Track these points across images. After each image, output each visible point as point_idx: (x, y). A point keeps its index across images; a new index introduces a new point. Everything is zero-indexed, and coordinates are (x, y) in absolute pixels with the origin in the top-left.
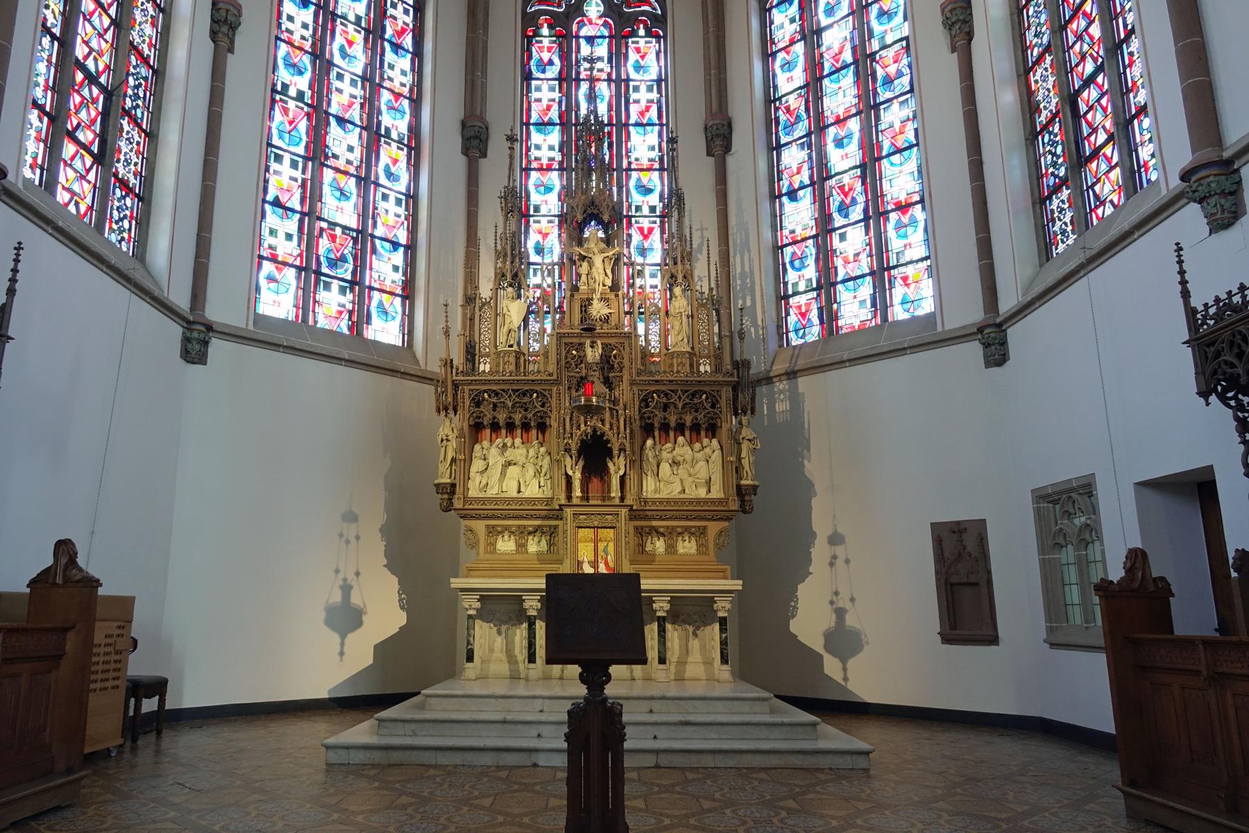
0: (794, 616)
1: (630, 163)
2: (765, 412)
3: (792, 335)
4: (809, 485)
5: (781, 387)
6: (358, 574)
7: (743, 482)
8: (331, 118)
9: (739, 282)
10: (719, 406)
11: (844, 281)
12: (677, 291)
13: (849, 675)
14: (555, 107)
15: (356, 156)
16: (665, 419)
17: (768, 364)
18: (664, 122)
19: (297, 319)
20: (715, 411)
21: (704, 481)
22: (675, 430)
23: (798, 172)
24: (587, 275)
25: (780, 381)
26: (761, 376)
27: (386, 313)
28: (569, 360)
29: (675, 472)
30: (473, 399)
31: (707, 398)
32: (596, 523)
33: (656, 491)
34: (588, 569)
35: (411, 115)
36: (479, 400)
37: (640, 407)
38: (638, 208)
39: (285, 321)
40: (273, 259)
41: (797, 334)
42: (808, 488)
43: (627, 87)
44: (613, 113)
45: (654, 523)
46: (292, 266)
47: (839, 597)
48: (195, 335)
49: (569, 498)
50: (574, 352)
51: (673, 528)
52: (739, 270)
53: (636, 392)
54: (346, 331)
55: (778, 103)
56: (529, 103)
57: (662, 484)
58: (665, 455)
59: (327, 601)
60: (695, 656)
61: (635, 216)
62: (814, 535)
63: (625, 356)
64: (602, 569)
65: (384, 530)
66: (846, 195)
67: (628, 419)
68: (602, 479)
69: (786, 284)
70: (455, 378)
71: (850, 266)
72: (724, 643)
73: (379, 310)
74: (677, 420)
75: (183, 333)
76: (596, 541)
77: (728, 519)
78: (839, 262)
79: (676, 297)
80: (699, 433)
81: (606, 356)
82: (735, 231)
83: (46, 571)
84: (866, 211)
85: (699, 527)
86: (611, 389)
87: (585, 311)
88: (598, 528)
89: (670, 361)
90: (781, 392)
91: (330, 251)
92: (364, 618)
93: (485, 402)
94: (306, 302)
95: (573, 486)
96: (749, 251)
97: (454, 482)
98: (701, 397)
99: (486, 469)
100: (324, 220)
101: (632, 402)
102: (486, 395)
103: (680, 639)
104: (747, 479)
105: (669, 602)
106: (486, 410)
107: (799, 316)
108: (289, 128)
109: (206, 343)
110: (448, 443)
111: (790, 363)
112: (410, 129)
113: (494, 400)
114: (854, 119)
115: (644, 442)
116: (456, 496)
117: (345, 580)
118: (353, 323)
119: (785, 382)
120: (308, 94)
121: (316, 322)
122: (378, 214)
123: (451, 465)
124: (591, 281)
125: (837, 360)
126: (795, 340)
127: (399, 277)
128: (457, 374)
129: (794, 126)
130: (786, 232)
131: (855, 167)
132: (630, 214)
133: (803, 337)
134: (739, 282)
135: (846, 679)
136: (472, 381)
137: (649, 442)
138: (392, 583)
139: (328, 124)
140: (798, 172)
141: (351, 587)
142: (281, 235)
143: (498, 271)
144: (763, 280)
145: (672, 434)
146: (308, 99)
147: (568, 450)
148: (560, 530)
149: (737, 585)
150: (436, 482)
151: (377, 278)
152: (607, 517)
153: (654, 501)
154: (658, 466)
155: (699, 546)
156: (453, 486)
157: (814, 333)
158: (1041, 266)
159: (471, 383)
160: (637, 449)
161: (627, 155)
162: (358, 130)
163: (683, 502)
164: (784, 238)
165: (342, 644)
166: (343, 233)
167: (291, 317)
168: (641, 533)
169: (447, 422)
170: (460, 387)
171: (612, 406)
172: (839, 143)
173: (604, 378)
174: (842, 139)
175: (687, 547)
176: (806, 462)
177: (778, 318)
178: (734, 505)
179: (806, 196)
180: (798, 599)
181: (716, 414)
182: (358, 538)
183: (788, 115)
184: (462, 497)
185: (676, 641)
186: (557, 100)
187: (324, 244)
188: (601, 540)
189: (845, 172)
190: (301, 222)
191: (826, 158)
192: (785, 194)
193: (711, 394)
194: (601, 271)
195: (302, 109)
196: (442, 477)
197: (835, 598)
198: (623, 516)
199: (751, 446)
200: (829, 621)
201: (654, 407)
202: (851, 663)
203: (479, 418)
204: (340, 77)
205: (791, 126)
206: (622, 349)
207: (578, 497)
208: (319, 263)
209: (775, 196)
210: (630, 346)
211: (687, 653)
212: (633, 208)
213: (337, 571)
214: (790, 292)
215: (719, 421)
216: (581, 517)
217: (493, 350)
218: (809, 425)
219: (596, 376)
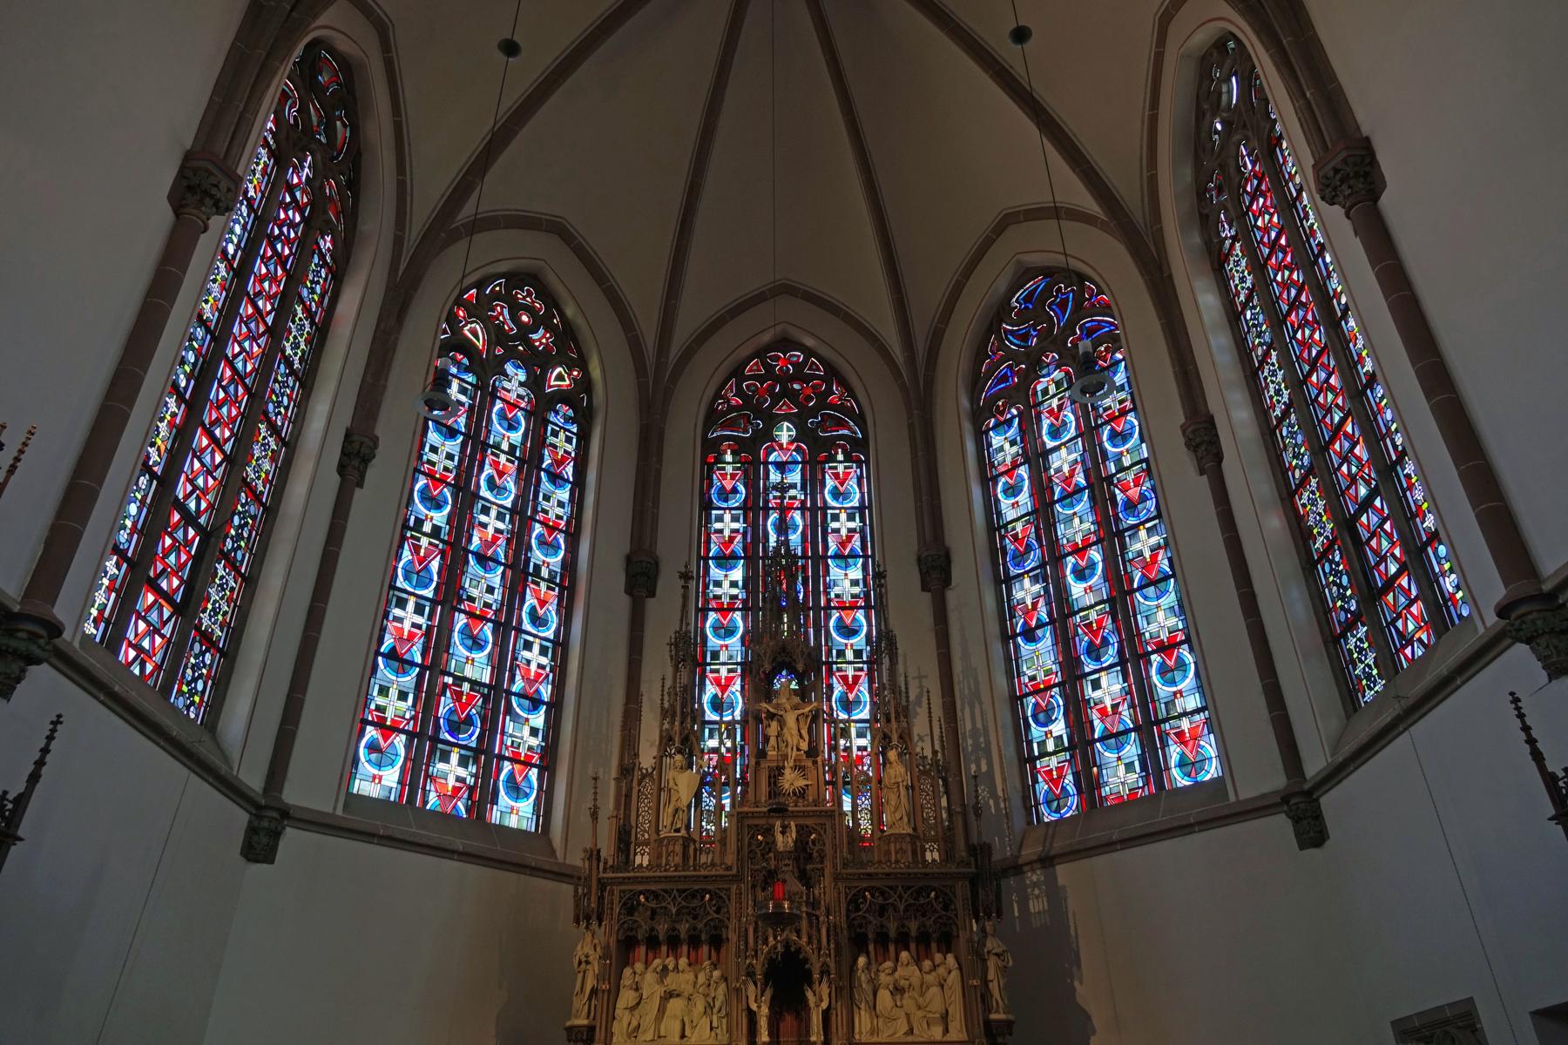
2: (1016, 914)
3: (1043, 809)
7: (993, 1016)
9: (970, 742)
16: (882, 926)
20: (949, 914)
22: (896, 942)
24: (777, 737)
25: (1033, 870)
28: (753, 847)
29: (898, 1004)
30: (625, 904)
31: (937, 897)
37: (848, 910)
41: (1049, 807)
43: (825, 516)
52: (969, 726)
58: (884, 978)
66: (1095, 633)
71: (1109, 719)
75: (250, 822)
79: (891, 763)
80: (928, 946)
81: (801, 841)
84: (1120, 652)
86: (809, 886)
87: (775, 783)
90: (1035, 885)
93: (641, 908)
94: (415, 774)
96: (981, 703)
97: (593, 1023)
98: (928, 896)
99: (638, 1004)
101: (837, 909)
104: (997, 1011)
106: (642, 920)
109: (276, 835)
111: (1044, 846)
115: (855, 961)
123: (590, 999)
128: (605, 870)
133: (1057, 811)
134: (970, 742)
136: (624, 878)
137: (862, 960)
139: (467, 562)
142: (394, 693)
143: (664, 734)
145: (892, 948)
147: (751, 974)
150: (568, 1024)
158: (1348, 717)
159: (623, 881)
171: (810, 911)
174: (1084, 569)
176: (1076, 983)
187: (446, 704)
190: (420, 677)
194: (795, 732)
195: (437, 546)
196: (577, 1017)
199: (1000, 963)
205: (1020, 558)
206: (822, 832)
208: (437, 727)
215: (954, 928)
217: (654, 836)
219: (788, 872)
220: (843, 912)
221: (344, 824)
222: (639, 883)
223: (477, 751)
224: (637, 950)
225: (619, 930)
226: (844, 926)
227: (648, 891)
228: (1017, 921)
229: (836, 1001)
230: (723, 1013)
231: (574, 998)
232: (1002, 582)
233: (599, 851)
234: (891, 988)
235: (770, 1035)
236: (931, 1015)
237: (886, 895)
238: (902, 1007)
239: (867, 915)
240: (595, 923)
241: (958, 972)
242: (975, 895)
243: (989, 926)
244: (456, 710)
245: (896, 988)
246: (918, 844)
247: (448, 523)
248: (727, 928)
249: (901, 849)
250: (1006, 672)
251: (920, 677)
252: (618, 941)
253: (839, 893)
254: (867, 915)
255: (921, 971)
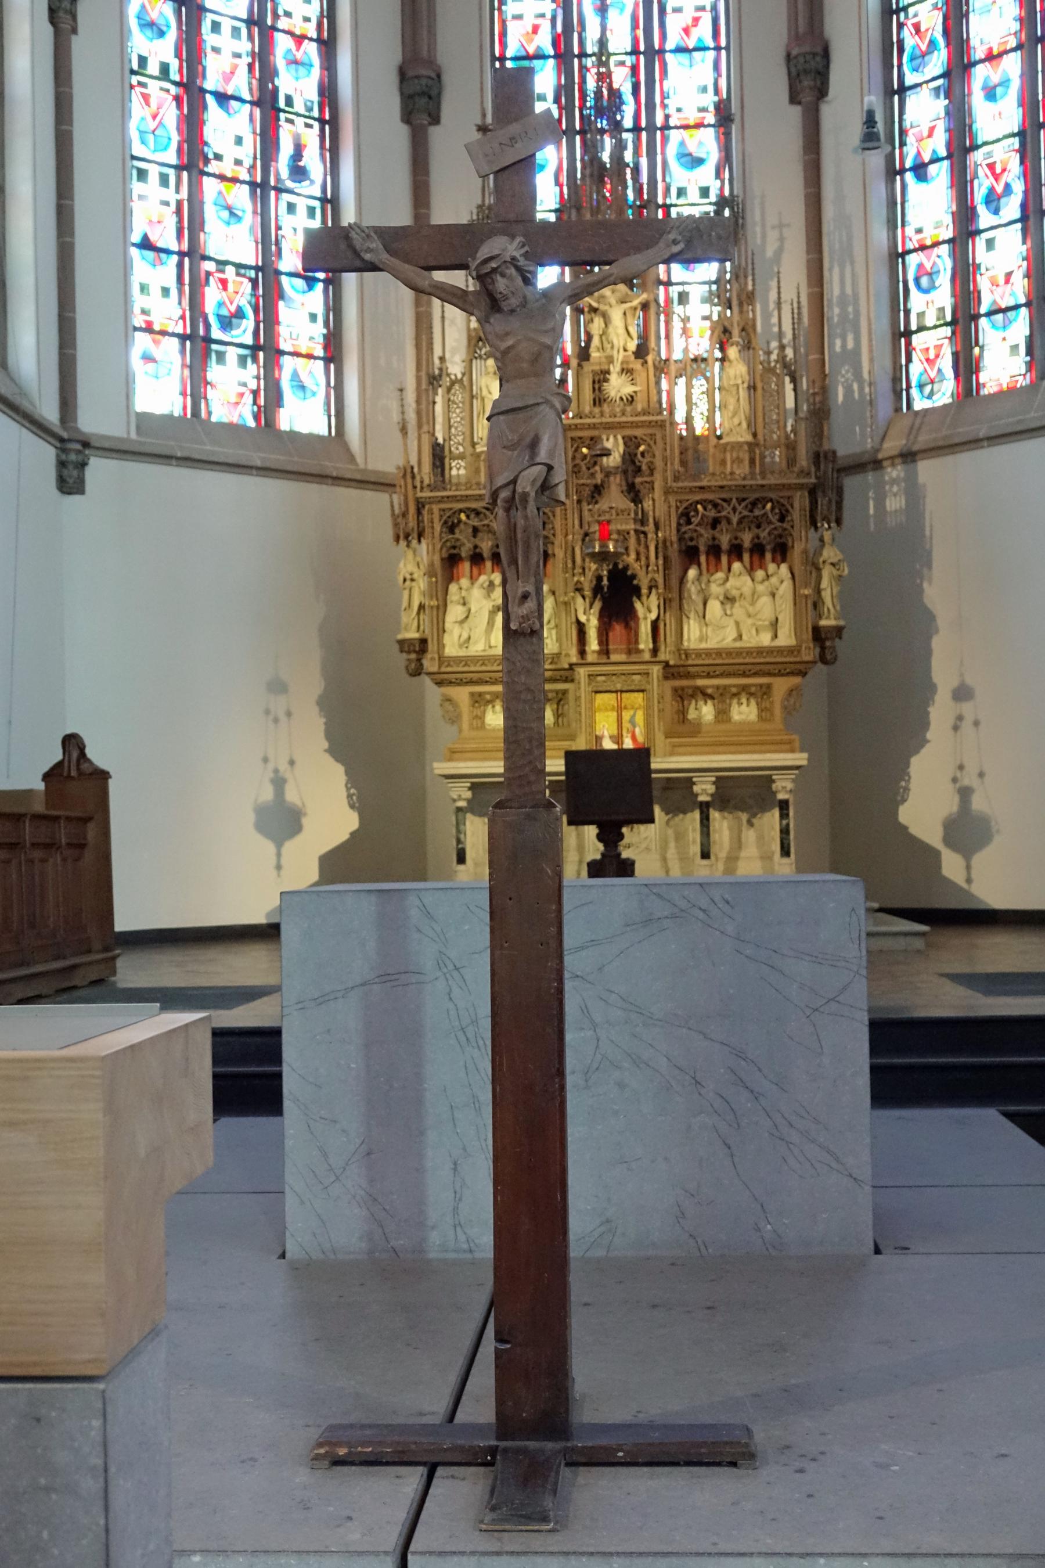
0: (904, 801)
1: (667, 117)
2: (872, 512)
3: (914, 392)
4: (931, 617)
5: (894, 474)
6: (292, 763)
7: (823, 623)
8: (208, 96)
9: (837, 311)
10: (789, 518)
11: (989, 314)
12: (733, 352)
13: (974, 875)
14: (546, 26)
15: (248, 151)
16: (714, 539)
17: (877, 439)
18: (723, 44)
19: (185, 414)
20: (785, 525)
21: (767, 623)
22: (730, 553)
23: (930, 135)
24: (601, 336)
25: (893, 465)
26: (866, 458)
27: (303, 387)
28: (578, 461)
29: (728, 612)
30: (446, 522)
31: (773, 509)
32: (619, 687)
33: (702, 638)
34: (608, 745)
35: (322, 68)
36: (453, 523)
37: (679, 525)
38: (681, 192)
39: (170, 417)
40: (149, 328)
41: (921, 392)
42: (927, 622)
44: (640, 33)
45: (700, 682)
46: (173, 335)
47: (964, 773)
48: (73, 457)
49: (582, 653)
50: (585, 450)
51: (725, 687)
52: (836, 292)
53: (673, 504)
54: (251, 423)
55: (902, 15)
56: (503, 23)
57: (710, 629)
58: (715, 589)
59: (256, 800)
60: (750, 850)
61: (676, 205)
62: (932, 688)
63: (657, 453)
64: (628, 744)
65: (324, 703)
66: (997, 177)
67: (660, 545)
68: (627, 626)
69: (907, 312)
70: (419, 494)
71: (1000, 290)
72: (785, 831)
73: (295, 383)
74: (730, 541)
75: (57, 456)
76: (620, 709)
77: (803, 674)
78: (983, 283)
79: (730, 361)
80: (762, 555)
81: (630, 454)
82: (832, 228)
83: (59, 765)
84: (1024, 206)
85: (761, 686)
86: (637, 499)
87: (600, 389)
88: (622, 691)
89: (722, 456)
90: (894, 482)
91: (221, 304)
92: (305, 821)
93: (462, 526)
95: (587, 636)
96: (852, 263)
97: (424, 637)
98: (764, 507)
99: (467, 617)
100: (210, 259)
101: (667, 523)
102: (463, 516)
103: (730, 829)
104: (828, 618)
105: (714, 783)
106: (463, 535)
107: (926, 364)
108: (153, 125)
109: (83, 465)
110: (414, 584)
111: (908, 440)
112: (321, 92)
113: (475, 522)
114: (1012, 55)
115: (685, 572)
116: (429, 656)
117: (276, 771)
118: (259, 407)
119: (899, 467)
120: (174, 64)
121: (209, 413)
122: (283, 236)
123: (418, 613)
124: (608, 346)
125: (970, 437)
126: (920, 404)
127: (319, 330)
128: (422, 488)
129: (926, 58)
130: (910, 231)
131: (1013, 135)
132: (668, 202)
133: (930, 396)
134: (837, 311)
135: (969, 881)
136: (443, 497)
137: (692, 573)
138: (337, 773)
139: (204, 107)
140: (930, 135)
141: (284, 781)
142: (155, 291)
143: (473, 334)
144: (872, 308)
145: (724, 559)
146: (175, 76)
147: (579, 590)
148: (571, 696)
149: (800, 758)
150: (400, 637)
151: (288, 337)
152: (634, 677)
153: (699, 654)
154: (705, 604)
155: (761, 710)
156: (424, 642)
157: (945, 392)
159: (442, 500)
160: (674, 582)
161: (662, 102)
162: (248, 106)
163: (739, 652)
164: (907, 240)
165: (279, 855)
166: (238, 274)
167: (177, 412)
168: (683, 697)
169: (410, 553)
170: (427, 507)
171: (639, 527)
172: (990, 93)
173: (628, 484)
174: (995, 87)
175: (744, 712)
176: (925, 585)
177: (894, 369)
178: (810, 652)
179: (941, 173)
180: (910, 777)
181: (785, 529)
182: (289, 714)
183: (916, 37)
184: (436, 656)
185: (726, 833)
186: (549, 16)
187: (212, 295)
188: (626, 708)
189: (998, 141)
190: (180, 266)
191: (970, 115)
192: (910, 169)
193: (778, 502)
194: (621, 331)
195: (168, 91)
196: (406, 629)
197: (959, 775)
198: (655, 676)
199: (835, 572)
200: (950, 805)
201: (699, 524)
202: (977, 859)
203: (454, 547)
204: (216, 27)
205: (921, 57)
206: (652, 443)
207: (594, 652)
208: (207, 326)
209: (893, 172)
210: (664, 437)
211: (740, 847)
212: (674, 192)
213: (266, 760)
214: (914, 327)
215: (790, 540)
216: (600, 678)
217: (470, 450)
218: (931, 530)
219: (616, 484)
220: (674, 525)
221: (142, 449)
222: (458, 501)
223: (255, 348)
224: (460, 566)
225: (441, 549)
226: (674, 538)
227: (468, 509)
228: (872, 520)
229: (665, 612)
230: (552, 624)
231: (403, 613)
232: (894, 93)
233: (412, 468)
234: (721, 598)
235: (600, 643)
236: (761, 623)
237: (719, 508)
238: (731, 615)
239: (698, 528)
240: (414, 542)
241: (791, 582)
242: (814, 504)
243: (827, 536)
244: (224, 303)
245: (727, 598)
246: (757, 452)
247: (178, 55)
248: (553, 543)
249: (738, 458)
250: (888, 221)
251: (781, 226)
252: (442, 559)
253: (669, 507)
254: (698, 528)
255: (753, 580)
